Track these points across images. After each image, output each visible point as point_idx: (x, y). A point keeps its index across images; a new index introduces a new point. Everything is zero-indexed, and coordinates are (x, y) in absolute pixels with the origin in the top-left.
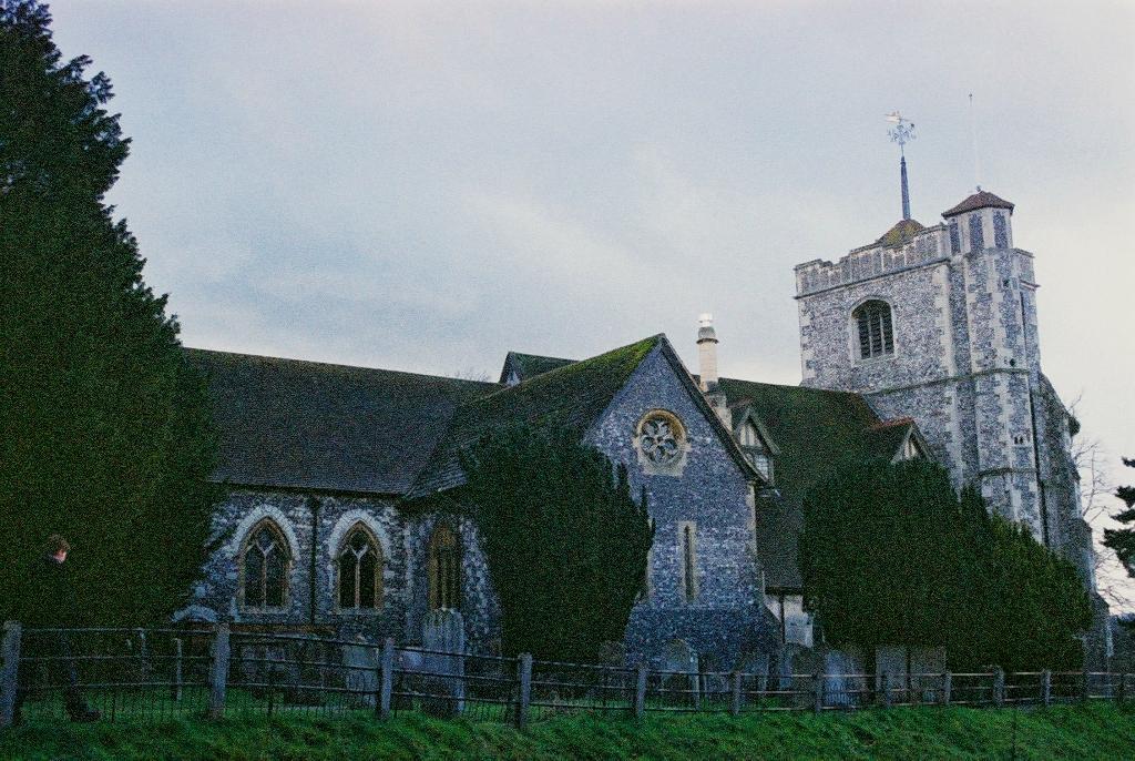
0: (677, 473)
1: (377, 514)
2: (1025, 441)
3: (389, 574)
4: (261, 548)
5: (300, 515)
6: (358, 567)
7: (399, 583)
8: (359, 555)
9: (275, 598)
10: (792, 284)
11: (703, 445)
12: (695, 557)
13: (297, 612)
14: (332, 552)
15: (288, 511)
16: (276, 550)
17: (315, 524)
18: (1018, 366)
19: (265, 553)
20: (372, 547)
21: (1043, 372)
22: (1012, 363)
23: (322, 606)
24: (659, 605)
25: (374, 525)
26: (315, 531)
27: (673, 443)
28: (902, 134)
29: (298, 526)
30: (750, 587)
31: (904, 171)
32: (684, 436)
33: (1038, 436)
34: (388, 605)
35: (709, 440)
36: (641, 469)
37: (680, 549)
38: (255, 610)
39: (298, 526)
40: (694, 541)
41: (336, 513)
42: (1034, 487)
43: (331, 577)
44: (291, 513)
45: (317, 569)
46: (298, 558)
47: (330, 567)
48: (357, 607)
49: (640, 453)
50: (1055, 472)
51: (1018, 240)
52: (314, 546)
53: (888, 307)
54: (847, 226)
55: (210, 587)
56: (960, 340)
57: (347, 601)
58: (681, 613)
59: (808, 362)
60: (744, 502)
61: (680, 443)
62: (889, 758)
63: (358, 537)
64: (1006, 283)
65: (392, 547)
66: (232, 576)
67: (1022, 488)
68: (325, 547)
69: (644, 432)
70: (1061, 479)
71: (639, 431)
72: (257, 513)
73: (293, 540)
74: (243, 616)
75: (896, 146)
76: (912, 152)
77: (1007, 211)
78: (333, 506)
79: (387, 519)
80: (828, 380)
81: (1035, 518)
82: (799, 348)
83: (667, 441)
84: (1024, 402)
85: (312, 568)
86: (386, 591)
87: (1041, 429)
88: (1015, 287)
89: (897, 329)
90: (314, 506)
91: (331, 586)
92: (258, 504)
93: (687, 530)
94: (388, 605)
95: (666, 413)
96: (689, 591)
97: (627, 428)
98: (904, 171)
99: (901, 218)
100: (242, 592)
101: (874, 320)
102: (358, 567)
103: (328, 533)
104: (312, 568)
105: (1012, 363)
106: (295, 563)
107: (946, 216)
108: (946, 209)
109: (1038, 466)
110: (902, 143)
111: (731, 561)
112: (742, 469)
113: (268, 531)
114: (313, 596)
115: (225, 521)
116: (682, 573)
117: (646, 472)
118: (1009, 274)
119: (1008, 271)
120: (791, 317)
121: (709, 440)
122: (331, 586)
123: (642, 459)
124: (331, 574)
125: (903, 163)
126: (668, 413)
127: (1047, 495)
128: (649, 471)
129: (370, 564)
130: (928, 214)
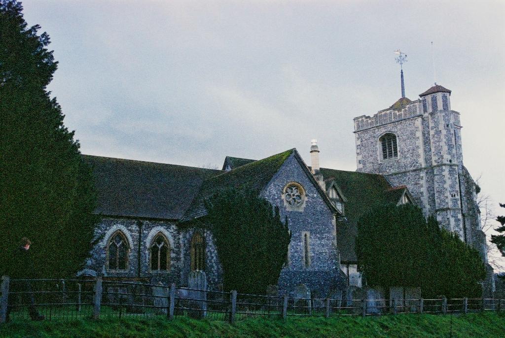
0: (301, 210)
1: (168, 228)
2: (456, 196)
3: (173, 255)
4: (116, 244)
5: (134, 229)
6: (159, 252)
7: (178, 259)
8: (160, 247)
9: (122, 266)
10: (352, 126)
11: (313, 198)
12: (309, 247)
13: (132, 272)
14: (148, 245)
15: (128, 227)
16: (123, 244)
17: (140, 233)
18: (453, 163)
19: (118, 246)
20: (165, 243)
21: (464, 165)
22: (450, 161)
23: (143, 269)
24: (293, 269)
25: (166, 233)
26: (140, 236)
27: (299, 197)
28: (401, 60)
29: (133, 234)
30: (334, 261)
31: (402, 76)
32: (304, 193)
33: (462, 194)
34: (173, 269)
35: (315, 195)
36: (285, 208)
37: (302, 244)
38: (113, 271)
39: (133, 234)
40: (309, 240)
41: (149, 228)
42: (460, 216)
43: (147, 256)
44: (130, 228)
45: (141, 253)
46: (133, 248)
47: (147, 252)
48: (159, 269)
49: (285, 201)
50: (469, 210)
51: (453, 107)
52: (140, 242)
53: (395, 137)
54: (377, 100)
55: (93, 261)
56: (427, 151)
57: (154, 267)
58: (303, 272)
59: (359, 161)
60: (331, 223)
61: (302, 197)
62: (396, 336)
63: (159, 238)
64: (448, 126)
65: (174, 243)
66: (103, 256)
67: (455, 217)
68: (145, 243)
69: (287, 192)
70: (472, 213)
71: (284, 191)
72: (114, 228)
73: (130, 240)
74: (108, 274)
75: (399, 65)
76: (406, 68)
77: (448, 94)
78: (148, 225)
79: (172, 231)
80: (368, 169)
81: (461, 230)
82: (356, 155)
83: (297, 196)
84: (456, 179)
85: (139, 252)
86: (172, 262)
87: (463, 191)
88: (452, 127)
89: (399, 146)
90: (140, 225)
91: (147, 260)
92: (115, 224)
93: (306, 235)
94: (173, 269)
95: (296, 184)
96: (307, 263)
97: (279, 190)
98: (402, 76)
99: (401, 97)
100: (108, 263)
101: (389, 142)
102: (159, 252)
103: (146, 237)
104: (139, 252)
105: (450, 161)
106: (131, 250)
107: (421, 96)
108: (421, 93)
109: (462, 207)
110: (401, 64)
111: (325, 249)
112: (330, 209)
113: (119, 236)
114: (139, 265)
115: (100, 231)
116: (304, 255)
117: (287, 210)
118: (449, 122)
119: (449, 120)
120: (352, 141)
121: (315, 195)
122: (147, 260)
123: (286, 204)
124: (147, 255)
125: (402, 72)
126: (297, 184)
127: (466, 220)
128: (289, 209)
129: (164, 251)
130: (413, 95)
